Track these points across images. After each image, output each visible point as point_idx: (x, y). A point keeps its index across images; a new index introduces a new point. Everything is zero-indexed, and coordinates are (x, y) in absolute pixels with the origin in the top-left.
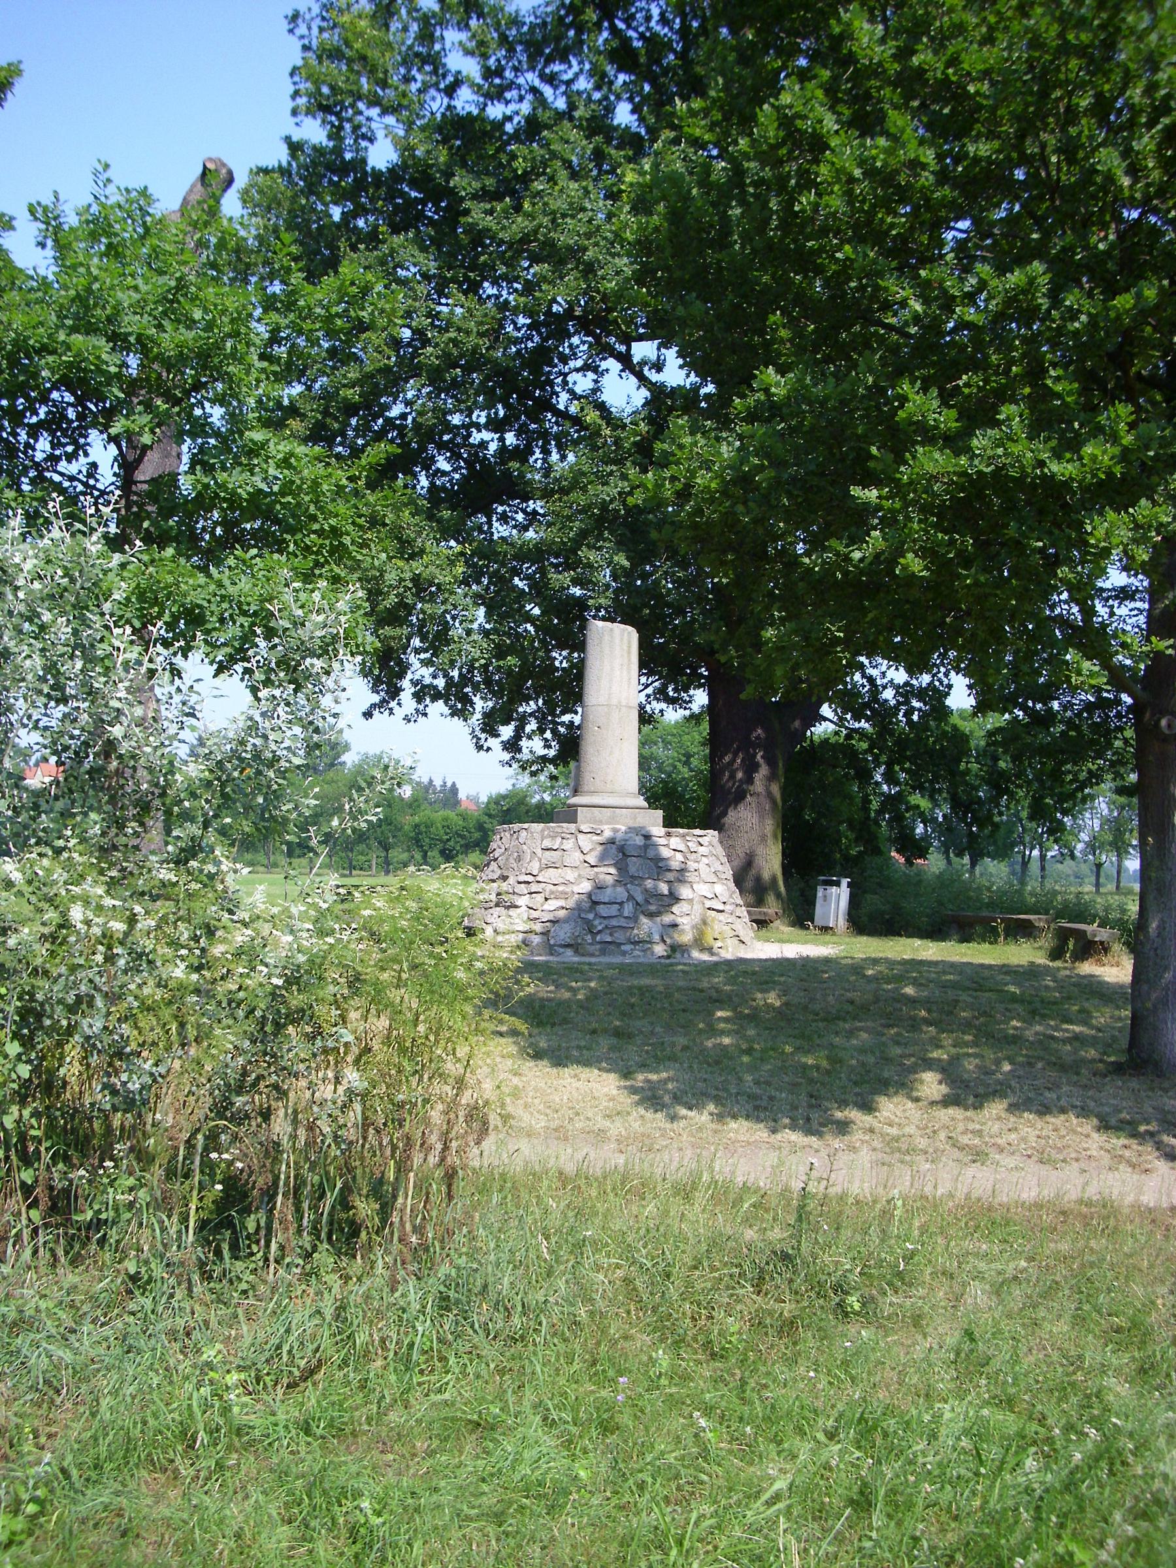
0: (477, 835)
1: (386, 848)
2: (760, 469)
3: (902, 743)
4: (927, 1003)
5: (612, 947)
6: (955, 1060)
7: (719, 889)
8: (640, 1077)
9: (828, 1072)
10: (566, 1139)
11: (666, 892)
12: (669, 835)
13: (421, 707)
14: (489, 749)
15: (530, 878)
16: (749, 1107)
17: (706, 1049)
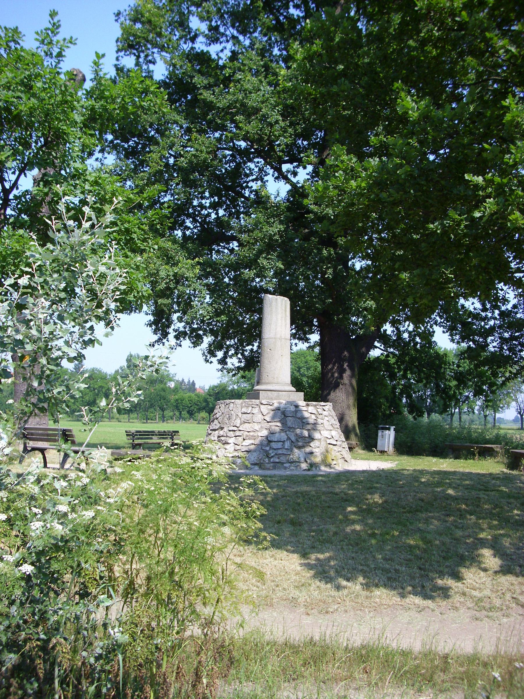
0: (204, 404)
1: (163, 410)
2: (401, 166)
3: (413, 359)
4: (465, 500)
5: (279, 465)
6: (496, 538)
7: (334, 433)
8: (313, 557)
9: (425, 551)
10: (272, 605)
11: (307, 435)
12: (308, 405)
13: (178, 342)
14: (211, 362)
15: (235, 429)
16: (384, 578)
17: (347, 534)
